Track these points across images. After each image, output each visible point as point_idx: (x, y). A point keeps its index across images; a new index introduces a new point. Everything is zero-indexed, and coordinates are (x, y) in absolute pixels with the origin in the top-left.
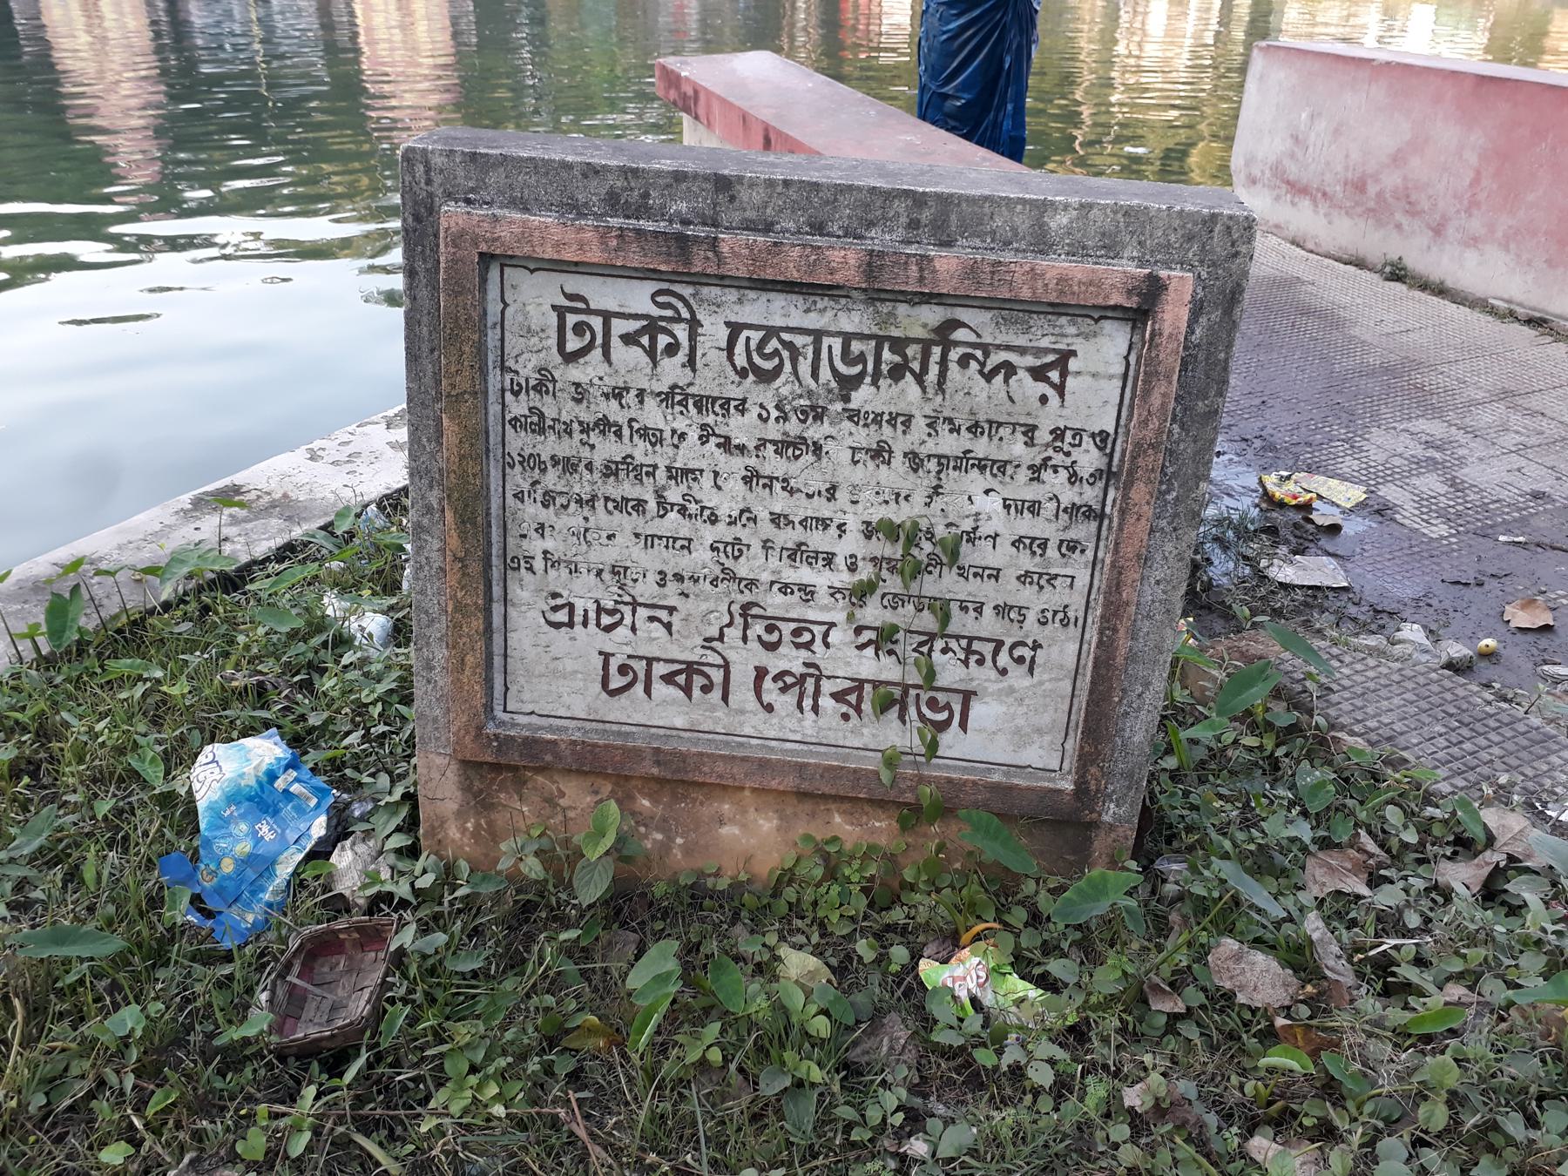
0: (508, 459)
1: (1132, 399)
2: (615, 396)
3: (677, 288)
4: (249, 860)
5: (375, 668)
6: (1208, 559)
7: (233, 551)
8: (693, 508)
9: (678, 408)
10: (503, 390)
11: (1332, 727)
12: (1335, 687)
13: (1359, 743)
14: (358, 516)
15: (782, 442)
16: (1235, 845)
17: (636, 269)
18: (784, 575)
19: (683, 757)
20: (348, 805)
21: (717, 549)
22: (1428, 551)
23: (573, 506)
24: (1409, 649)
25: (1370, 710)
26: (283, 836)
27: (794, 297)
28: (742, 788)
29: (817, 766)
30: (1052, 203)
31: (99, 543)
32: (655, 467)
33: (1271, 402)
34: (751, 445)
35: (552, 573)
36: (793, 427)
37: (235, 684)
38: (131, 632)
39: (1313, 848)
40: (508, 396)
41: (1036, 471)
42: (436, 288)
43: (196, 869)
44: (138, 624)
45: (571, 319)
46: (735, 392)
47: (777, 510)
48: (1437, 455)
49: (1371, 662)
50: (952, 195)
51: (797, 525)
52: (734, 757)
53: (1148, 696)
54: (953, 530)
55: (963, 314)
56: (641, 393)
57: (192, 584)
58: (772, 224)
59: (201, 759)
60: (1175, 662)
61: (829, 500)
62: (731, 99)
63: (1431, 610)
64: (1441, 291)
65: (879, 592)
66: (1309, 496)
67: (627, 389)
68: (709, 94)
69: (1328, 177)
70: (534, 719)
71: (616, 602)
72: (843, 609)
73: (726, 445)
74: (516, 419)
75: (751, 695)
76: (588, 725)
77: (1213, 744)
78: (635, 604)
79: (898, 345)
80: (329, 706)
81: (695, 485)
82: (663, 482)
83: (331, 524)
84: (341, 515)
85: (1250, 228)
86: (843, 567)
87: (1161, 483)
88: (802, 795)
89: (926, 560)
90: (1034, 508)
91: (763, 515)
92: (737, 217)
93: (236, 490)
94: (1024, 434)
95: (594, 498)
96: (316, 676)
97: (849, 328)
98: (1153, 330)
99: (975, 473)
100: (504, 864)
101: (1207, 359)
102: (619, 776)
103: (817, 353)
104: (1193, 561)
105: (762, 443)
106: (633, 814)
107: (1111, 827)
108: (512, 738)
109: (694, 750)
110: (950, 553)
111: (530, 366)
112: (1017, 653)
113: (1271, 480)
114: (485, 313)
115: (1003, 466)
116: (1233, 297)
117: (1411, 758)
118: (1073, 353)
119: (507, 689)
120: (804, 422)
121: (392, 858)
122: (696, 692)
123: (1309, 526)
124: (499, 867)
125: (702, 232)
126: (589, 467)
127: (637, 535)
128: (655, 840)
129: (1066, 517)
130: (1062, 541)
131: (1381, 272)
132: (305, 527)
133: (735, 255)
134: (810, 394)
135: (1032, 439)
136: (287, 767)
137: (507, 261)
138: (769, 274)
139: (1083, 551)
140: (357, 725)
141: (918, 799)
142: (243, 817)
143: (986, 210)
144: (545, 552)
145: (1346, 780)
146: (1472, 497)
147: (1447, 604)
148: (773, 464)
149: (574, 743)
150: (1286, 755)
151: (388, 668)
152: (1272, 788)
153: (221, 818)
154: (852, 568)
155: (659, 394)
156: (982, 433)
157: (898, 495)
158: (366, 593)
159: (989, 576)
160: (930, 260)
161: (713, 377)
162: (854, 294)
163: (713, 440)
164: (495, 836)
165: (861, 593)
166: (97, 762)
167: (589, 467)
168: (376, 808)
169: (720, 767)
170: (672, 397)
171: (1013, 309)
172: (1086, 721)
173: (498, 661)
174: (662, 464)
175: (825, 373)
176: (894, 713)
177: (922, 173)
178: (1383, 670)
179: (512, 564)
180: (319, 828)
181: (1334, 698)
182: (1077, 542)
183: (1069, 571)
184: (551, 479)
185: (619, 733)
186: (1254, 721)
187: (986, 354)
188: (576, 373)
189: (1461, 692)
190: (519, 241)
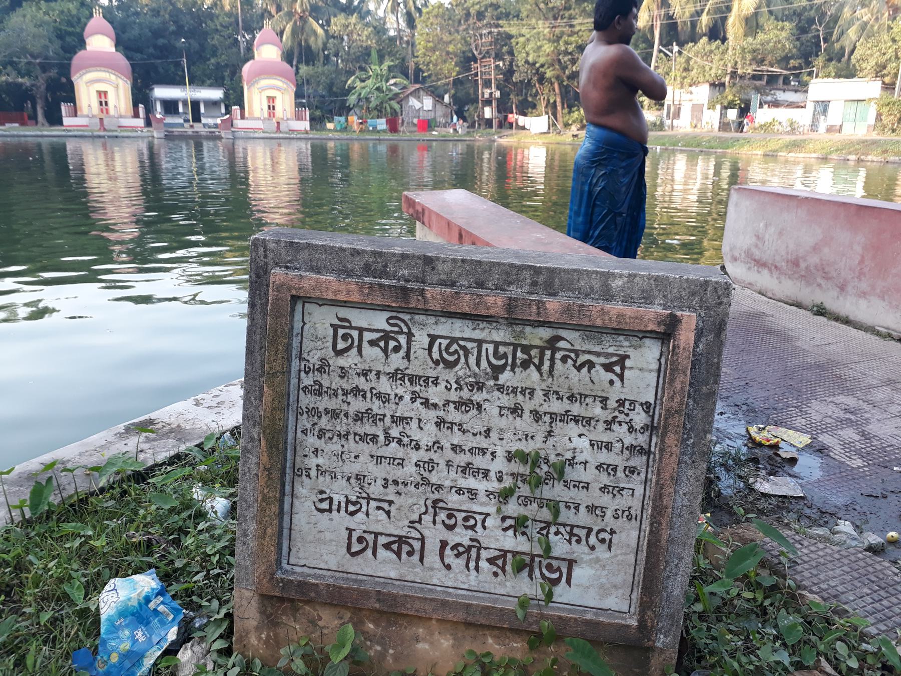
0: (300, 410)
1: (664, 384)
2: (363, 375)
3: (401, 316)
4: (126, 655)
5: (218, 532)
6: (718, 477)
7: (145, 458)
8: (405, 440)
9: (399, 382)
10: (300, 371)
11: (799, 587)
12: (799, 561)
13: (816, 598)
14: (218, 439)
15: (459, 402)
16: (741, 666)
17: (378, 305)
18: (459, 482)
19: (394, 597)
20: (193, 619)
21: (419, 466)
22: (852, 475)
23: (335, 438)
24: (844, 537)
25: (822, 577)
26: (150, 639)
27: (467, 321)
28: (431, 619)
29: (477, 606)
30: (613, 274)
31: (68, 452)
32: (384, 415)
33: (751, 384)
34: (441, 404)
35: (321, 478)
36: (465, 394)
37: (134, 540)
38: (80, 507)
39: (791, 669)
40: (303, 374)
41: (609, 424)
42: (266, 314)
43: (95, 659)
44: (84, 501)
45: (341, 332)
46: (432, 373)
47: (455, 442)
48: (853, 417)
49: (821, 546)
50: (556, 269)
51: (467, 452)
52: (426, 599)
53: (682, 566)
54: (560, 458)
55: (563, 333)
56: (378, 373)
57: (119, 477)
58: (455, 282)
59: (107, 588)
60: (698, 541)
61: (486, 437)
62: (442, 214)
63: (856, 513)
64: (847, 321)
65: (516, 495)
66: (776, 440)
67: (371, 371)
68: (430, 211)
69: (778, 258)
70: (305, 570)
71: (358, 497)
72: (494, 505)
73: (426, 403)
74: (306, 387)
75: (438, 559)
76: (338, 575)
77: (724, 596)
78: (369, 499)
79: (526, 349)
80: (188, 555)
81: (407, 427)
82: (389, 424)
83: (202, 443)
84: (208, 438)
85: (728, 288)
86: (494, 478)
87: (683, 434)
88: (468, 625)
89: (544, 476)
90: (608, 446)
91: (447, 446)
92: (435, 278)
93: (151, 422)
94: (601, 402)
95: (348, 434)
96: (183, 536)
97: (498, 339)
98: (674, 345)
99: (572, 424)
100: (282, 664)
101: (707, 362)
102: (355, 608)
103: (479, 352)
104: (707, 478)
105: (448, 402)
106: (363, 633)
107: (662, 651)
108: (292, 581)
109: (401, 593)
110: (559, 472)
111: (316, 357)
112: (601, 536)
113: (753, 430)
114: (292, 328)
115: (589, 420)
116: (719, 328)
117: (850, 610)
118: (628, 357)
119: (290, 550)
120: (472, 391)
121: (215, 656)
122: (404, 556)
123: (778, 459)
124: (279, 665)
125: (416, 286)
126: (346, 415)
127: (372, 456)
128: (376, 650)
129: (628, 452)
130: (626, 467)
131: (811, 310)
132: (188, 445)
133: (433, 298)
134: (475, 375)
135: (605, 405)
136: (157, 595)
137: (307, 300)
138: (452, 309)
139: (639, 474)
140: (203, 568)
141: (540, 629)
142: (127, 626)
143: (575, 277)
144: (318, 466)
145: (810, 623)
146: (875, 443)
147: (865, 509)
148: (453, 415)
149: (328, 586)
150: (771, 605)
151: (225, 532)
152: (763, 627)
153: (114, 626)
154: (500, 479)
155: (389, 374)
156: (576, 401)
157: (527, 436)
158: (218, 485)
159: (583, 487)
160: (543, 303)
161: (420, 365)
162: (501, 320)
163: (419, 401)
164: (278, 645)
165: (505, 495)
166: (46, 588)
167: (346, 415)
168: (209, 622)
169: (417, 605)
170: (396, 376)
171: (592, 331)
172: (644, 581)
173: (286, 532)
174: (389, 414)
175: (484, 364)
176: (525, 573)
177: (540, 256)
178: (829, 551)
179: (298, 473)
180: (172, 634)
181: (799, 568)
182: (635, 468)
183: (630, 486)
184: (324, 422)
185: (356, 581)
186: (749, 582)
187: (577, 356)
188: (342, 361)
189: (878, 567)
190: (314, 289)
